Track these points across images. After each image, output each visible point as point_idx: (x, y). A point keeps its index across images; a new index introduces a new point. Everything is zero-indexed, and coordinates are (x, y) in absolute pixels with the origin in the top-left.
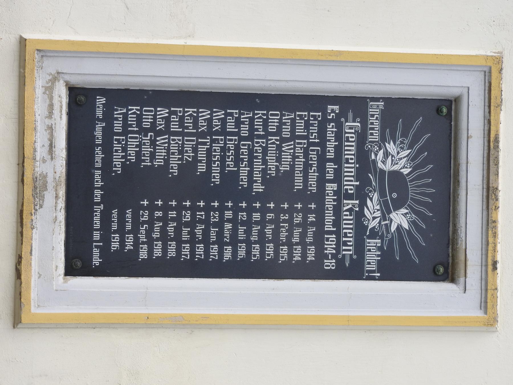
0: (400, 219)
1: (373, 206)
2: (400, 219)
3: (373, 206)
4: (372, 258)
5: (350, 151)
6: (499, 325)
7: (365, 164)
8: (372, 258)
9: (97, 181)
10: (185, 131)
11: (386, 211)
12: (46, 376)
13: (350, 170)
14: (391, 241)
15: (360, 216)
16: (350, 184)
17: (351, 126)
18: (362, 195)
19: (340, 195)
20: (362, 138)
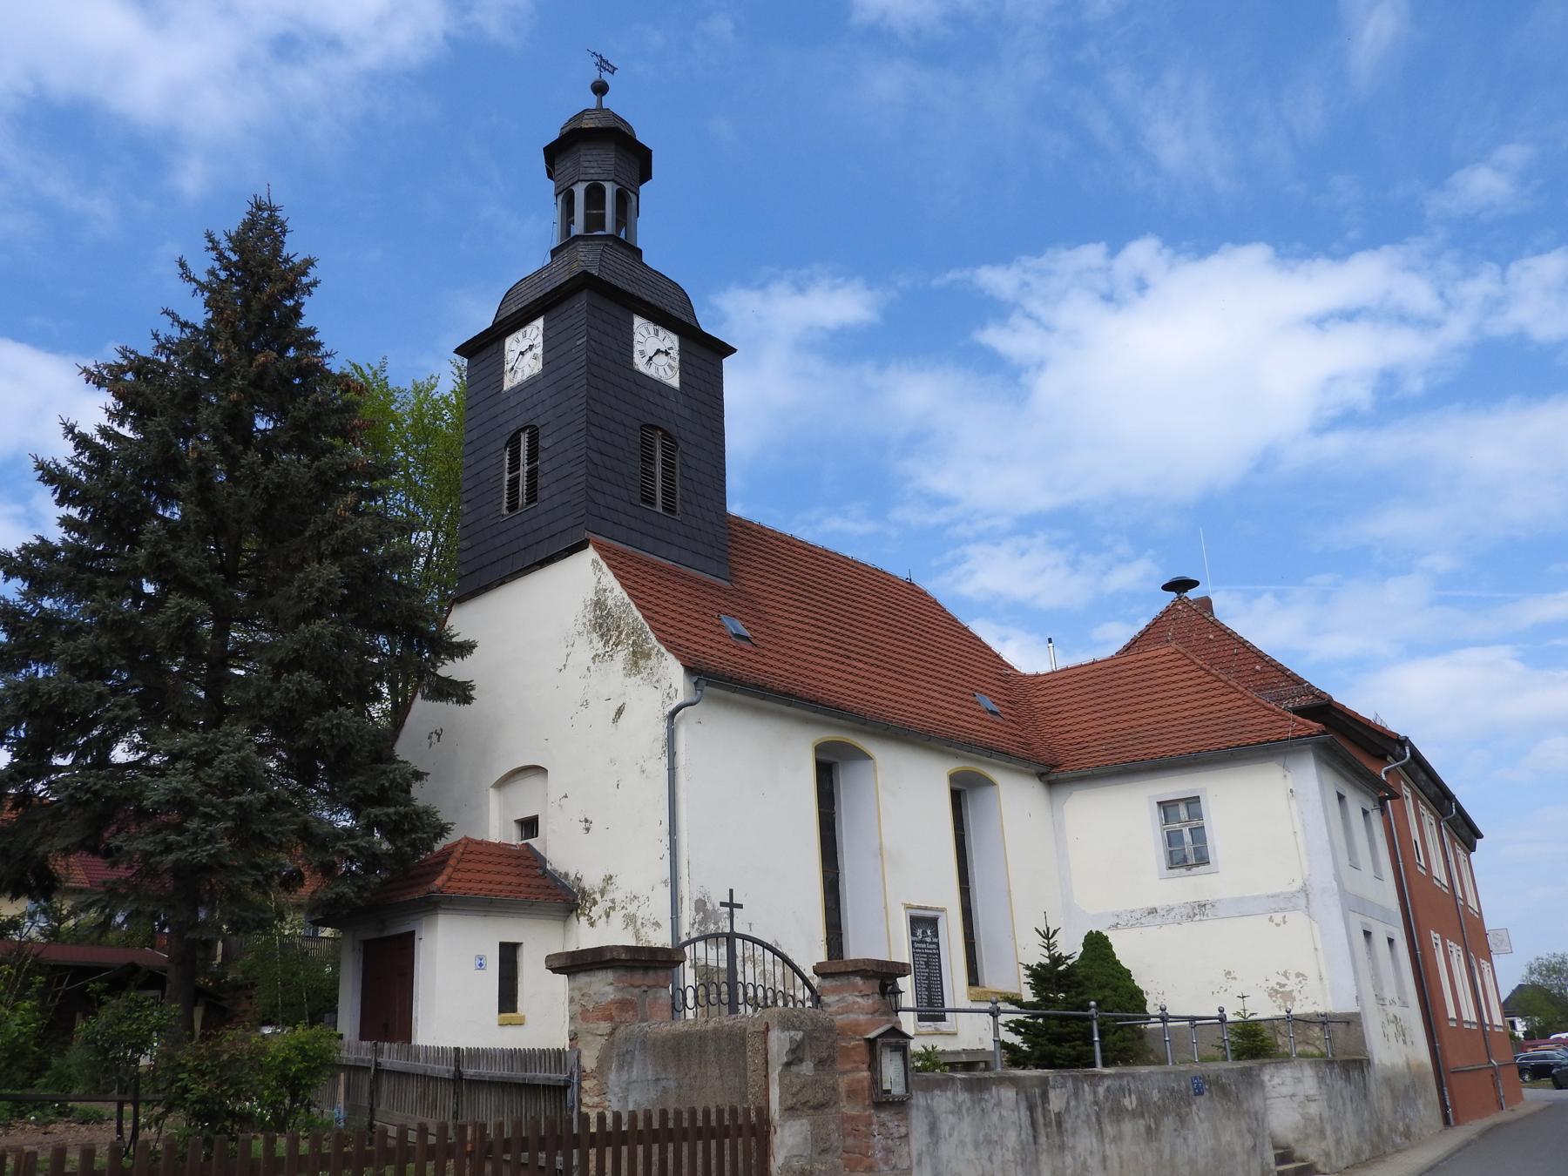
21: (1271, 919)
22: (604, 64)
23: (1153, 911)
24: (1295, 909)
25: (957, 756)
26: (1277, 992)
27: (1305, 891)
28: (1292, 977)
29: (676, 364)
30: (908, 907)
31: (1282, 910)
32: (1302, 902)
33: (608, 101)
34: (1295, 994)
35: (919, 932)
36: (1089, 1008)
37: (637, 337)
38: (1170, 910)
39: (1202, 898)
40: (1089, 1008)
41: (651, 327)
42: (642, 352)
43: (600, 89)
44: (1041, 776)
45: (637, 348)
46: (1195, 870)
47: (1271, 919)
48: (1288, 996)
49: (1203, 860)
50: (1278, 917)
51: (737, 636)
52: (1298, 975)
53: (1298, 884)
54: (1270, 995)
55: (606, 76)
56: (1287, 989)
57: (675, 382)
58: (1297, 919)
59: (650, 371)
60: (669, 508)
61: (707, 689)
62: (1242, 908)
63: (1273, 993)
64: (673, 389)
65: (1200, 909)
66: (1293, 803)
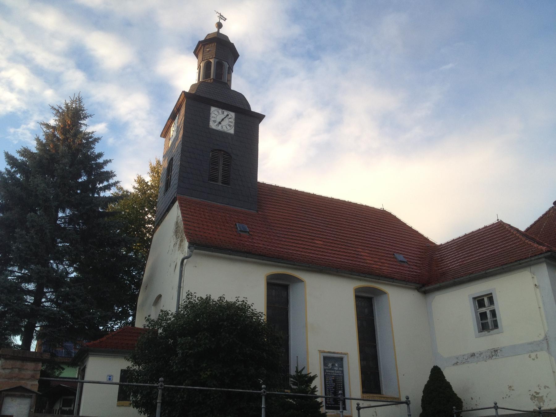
2: (336, 365)
4: (341, 369)
8: (341, 369)
16: (333, 371)
18: (334, 370)
21: (530, 357)
22: (221, 17)
23: (473, 355)
24: (542, 350)
25: (360, 280)
26: (535, 397)
27: (546, 339)
28: (542, 388)
29: (233, 124)
30: (321, 352)
31: (536, 351)
32: (545, 345)
33: (222, 31)
34: (544, 398)
35: (330, 365)
36: (261, 389)
37: (212, 115)
38: (481, 354)
39: (495, 347)
40: (261, 389)
41: (220, 111)
42: (215, 121)
43: (219, 25)
44: (418, 289)
45: (212, 119)
46: (492, 332)
47: (530, 357)
48: (541, 399)
49: (496, 326)
50: (533, 355)
51: (401, 261)
52: (545, 387)
53: (542, 337)
54: (531, 399)
55: (222, 21)
56: (540, 395)
57: (232, 131)
58: (543, 355)
59: (219, 128)
60: (226, 181)
61: (195, 251)
62: (514, 350)
63: (533, 397)
64: (230, 134)
65: (495, 353)
66: (538, 290)
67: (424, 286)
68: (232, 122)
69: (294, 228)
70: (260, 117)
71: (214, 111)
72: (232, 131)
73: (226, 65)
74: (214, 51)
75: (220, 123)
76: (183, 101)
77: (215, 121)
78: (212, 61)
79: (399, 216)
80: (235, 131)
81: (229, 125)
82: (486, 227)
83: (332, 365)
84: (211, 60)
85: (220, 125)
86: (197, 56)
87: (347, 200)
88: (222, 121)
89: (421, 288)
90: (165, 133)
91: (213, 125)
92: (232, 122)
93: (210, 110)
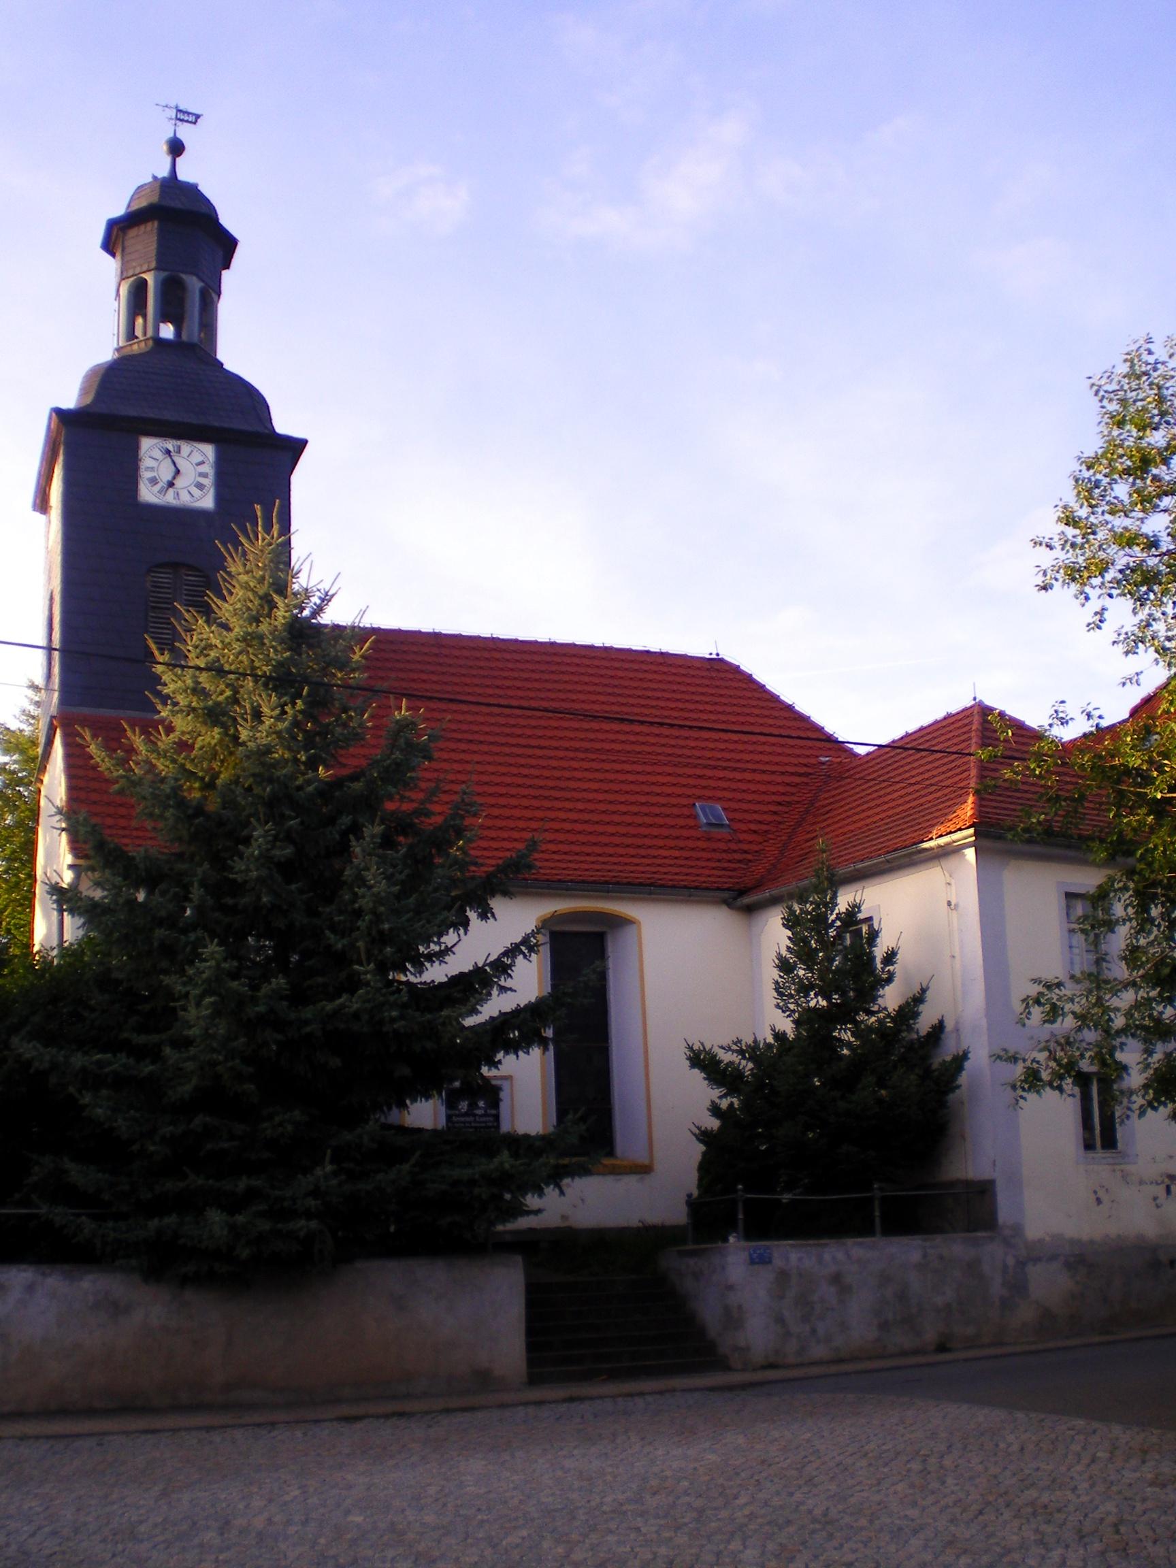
0: (481, 1104)
1: (479, 1112)
2: (481, 1104)
3: (479, 1112)
4: (493, 1112)
5: (462, 1119)
6: (165, 148)
7: (466, 1114)
8: (493, 1112)
9: (800, 1259)
10: (329, 1152)
11: (480, 1108)
12: (1158, 1206)
13: (468, 1119)
14: (236, 551)
15: (481, 1116)
16: (471, 1119)
17: (454, 1119)
18: (475, 1115)
19: (475, 1121)
20: (458, 1116)
29: (208, 482)
37: (146, 462)
42: (154, 481)
44: (728, 903)
45: (145, 475)
59: (169, 499)
67: (742, 892)
68: (205, 475)
69: (549, 686)
70: (296, 447)
71: (150, 448)
72: (207, 502)
73: (194, 284)
74: (152, 247)
75: (171, 484)
76: (58, 432)
77: (154, 481)
78: (150, 278)
79: (761, 676)
80: (219, 498)
81: (200, 486)
82: (949, 716)
83: (470, 1105)
84: (143, 276)
85: (171, 491)
86: (113, 255)
87: (598, 643)
88: (176, 474)
89: (735, 899)
90: (42, 504)
91: (148, 494)
92: (205, 475)
93: (136, 448)
